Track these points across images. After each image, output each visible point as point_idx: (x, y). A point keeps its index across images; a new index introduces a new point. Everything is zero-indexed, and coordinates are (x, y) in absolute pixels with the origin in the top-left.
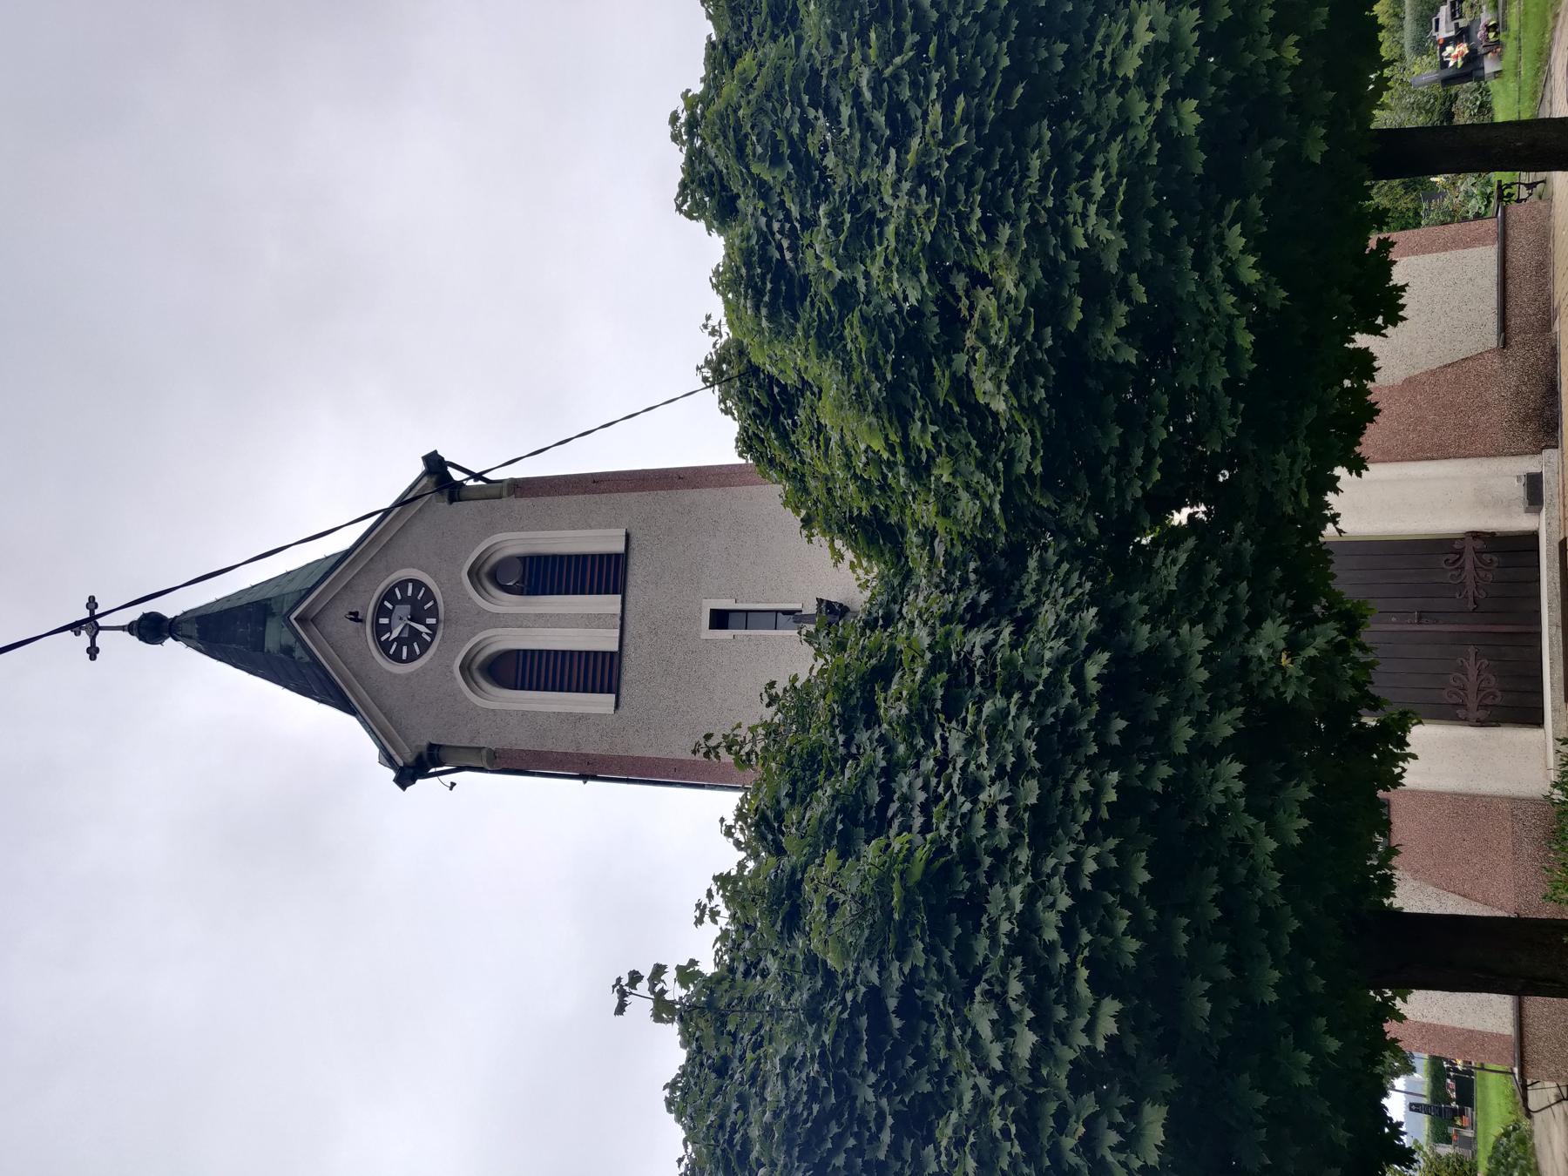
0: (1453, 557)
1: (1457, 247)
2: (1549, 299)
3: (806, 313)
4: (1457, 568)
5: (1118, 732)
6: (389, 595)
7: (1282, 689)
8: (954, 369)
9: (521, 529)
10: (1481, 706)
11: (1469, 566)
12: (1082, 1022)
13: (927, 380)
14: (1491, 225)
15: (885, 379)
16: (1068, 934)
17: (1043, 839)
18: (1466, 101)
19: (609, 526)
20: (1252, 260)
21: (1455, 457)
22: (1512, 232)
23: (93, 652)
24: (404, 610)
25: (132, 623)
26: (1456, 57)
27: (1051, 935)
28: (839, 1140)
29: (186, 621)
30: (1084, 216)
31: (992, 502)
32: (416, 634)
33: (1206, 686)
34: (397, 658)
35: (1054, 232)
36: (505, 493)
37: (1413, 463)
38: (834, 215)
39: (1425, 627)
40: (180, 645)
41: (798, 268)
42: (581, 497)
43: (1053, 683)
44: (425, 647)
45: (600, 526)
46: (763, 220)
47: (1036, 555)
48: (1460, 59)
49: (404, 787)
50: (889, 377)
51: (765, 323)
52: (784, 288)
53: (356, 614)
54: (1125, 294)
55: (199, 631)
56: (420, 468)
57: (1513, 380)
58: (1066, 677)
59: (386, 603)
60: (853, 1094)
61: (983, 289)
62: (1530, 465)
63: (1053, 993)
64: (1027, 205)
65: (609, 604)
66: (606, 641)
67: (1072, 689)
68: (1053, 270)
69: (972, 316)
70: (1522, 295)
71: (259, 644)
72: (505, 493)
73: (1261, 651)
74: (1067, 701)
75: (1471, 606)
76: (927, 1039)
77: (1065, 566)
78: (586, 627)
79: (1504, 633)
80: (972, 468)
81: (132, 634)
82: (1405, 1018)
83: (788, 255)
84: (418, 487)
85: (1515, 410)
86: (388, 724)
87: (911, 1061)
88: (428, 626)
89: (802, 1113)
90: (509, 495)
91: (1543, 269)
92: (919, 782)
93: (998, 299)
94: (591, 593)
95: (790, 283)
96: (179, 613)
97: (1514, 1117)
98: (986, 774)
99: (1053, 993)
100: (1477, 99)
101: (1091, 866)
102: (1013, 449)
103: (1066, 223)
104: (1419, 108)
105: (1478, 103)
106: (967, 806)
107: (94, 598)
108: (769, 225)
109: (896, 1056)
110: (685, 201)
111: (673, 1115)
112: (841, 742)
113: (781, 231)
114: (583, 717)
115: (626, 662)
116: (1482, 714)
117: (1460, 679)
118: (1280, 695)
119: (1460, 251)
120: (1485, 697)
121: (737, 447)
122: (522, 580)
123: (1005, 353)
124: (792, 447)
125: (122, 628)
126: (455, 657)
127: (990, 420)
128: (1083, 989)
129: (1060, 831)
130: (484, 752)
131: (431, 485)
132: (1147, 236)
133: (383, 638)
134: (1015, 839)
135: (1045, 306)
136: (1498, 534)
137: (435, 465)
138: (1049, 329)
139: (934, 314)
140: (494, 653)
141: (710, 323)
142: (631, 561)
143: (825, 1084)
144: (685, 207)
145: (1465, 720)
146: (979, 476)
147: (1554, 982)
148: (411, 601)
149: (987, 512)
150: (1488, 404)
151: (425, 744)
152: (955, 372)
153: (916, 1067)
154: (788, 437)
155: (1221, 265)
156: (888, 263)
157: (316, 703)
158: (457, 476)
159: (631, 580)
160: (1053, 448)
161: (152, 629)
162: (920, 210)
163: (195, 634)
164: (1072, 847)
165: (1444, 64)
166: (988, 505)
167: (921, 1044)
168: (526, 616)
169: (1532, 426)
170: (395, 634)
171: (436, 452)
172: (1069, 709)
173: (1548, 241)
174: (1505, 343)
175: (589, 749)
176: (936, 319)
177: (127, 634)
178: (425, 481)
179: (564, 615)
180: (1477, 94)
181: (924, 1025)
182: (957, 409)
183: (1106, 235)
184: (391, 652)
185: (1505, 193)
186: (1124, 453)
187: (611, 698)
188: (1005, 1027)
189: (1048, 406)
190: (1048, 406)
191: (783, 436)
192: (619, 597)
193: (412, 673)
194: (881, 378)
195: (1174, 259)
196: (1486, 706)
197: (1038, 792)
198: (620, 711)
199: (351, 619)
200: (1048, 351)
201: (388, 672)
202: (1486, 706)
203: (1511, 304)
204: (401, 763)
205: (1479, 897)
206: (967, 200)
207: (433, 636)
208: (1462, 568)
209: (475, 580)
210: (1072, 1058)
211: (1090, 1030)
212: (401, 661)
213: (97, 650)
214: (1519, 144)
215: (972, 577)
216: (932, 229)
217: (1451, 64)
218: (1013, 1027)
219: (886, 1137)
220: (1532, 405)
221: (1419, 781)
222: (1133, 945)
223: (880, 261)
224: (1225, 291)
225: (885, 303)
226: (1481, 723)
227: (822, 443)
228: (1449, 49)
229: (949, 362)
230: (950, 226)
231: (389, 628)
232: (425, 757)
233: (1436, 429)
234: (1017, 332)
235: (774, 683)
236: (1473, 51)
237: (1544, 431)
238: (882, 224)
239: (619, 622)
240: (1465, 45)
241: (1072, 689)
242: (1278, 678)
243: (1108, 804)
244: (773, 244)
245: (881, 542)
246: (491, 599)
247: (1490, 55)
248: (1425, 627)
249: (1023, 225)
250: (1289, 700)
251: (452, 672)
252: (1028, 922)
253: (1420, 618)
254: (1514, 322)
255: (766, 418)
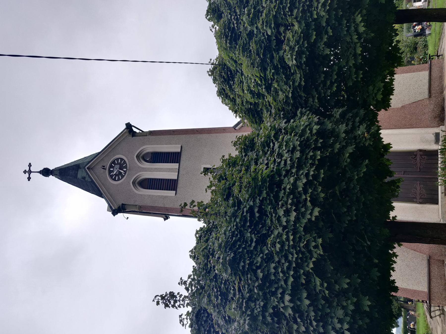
0: (414, 156)
1: (417, 71)
2: (443, 85)
3: (240, 42)
4: (415, 160)
5: (320, 143)
6: (113, 162)
7: (365, 143)
8: (279, 55)
9: (152, 145)
10: (420, 198)
11: (418, 159)
12: (309, 212)
13: (272, 57)
14: (427, 65)
15: (261, 57)
16: (305, 191)
17: (299, 168)
18: (421, 44)
19: (176, 144)
20: (363, 24)
21: (415, 128)
22: (432, 67)
23: (29, 179)
24: (118, 166)
25: (41, 171)
26: (418, 29)
27: (300, 189)
28: (240, 246)
29: (56, 170)
30: (317, 8)
31: (288, 93)
32: (120, 173)
33: (344, 138)
34: (114, 180)
35: (309, 12)
36: (148, 135)
37: (403, 129)
38: (249, 11)
39: (405, 176)
40: (54, 177)
41: (238, 30)
42: (169, 136)
43: (304, 131)
44: (123, 176)
45: (174, 144)
46: (230, 16)
47: (300, 110)
48: (419, 30)
49: (114, 215)
50: (262, 56)
51: (228, 45)
52: (234, 35)
53: (104, 166)
54: (327, 33)
55: (59, 173)
56: (124, 127)
57: (432, 107)
58: (307, 129)
59: (113, 165)
60: (244, 236)
61: (288, 31)
62: (437, 130)
63: (301, 205)
64: (302, 4)
65: (176, 166)
66: (173, 176)
67: (309, 132)
68: (308, 25)
69: (285, 39)
70: (435, 85)
71: (76, 177)
72: (148, 135)
73: (359, 132)
74: (307, 135)
75: (419, 170)
76: (265, 221)
77: (308, 112)
78: (169, 172)
79: (428, 178)
80: (283, 84)
81: (40, 174)
82: (396, 262)
83: (235, 25)
84: (124, 132)
85: (433, 115)
86: (111, 197)
87: (261, 226)
88: (124, 171)
89: (230, 240)
90: (149, 135)
91: (441, 77)
92: (266, 158)
93: (293, 33)
94: (170, 163)
95: (235, 35)
96: (54, 168)
97: (427, 331)
98: (285, 152)
99: (301, 205)
100: (424, 43)
101: (312, 173)
102: (295, 78)
103: (312, 10)
104: (407, 46)
105: (424, 44)
106: (279, 160)
107: (30, 163)
108: (231, 17)
109: (256, 224)
110: (208, 16)
111: (192, 259)
112: (243, 155)
113: (234, 19)
114: (166, 197)
115: (179, 181)
116: (421, 200)
117: (415, 191)
118: (364, 145)
119: (418, 73)
120: (422, 196)
121: (217, 93)
122: (151, 159)
123: (294, 48)
124: (233, 90)
125: (38, 172)
126: (131, 179)
127: (289, 70)
128: (309, 204)
129: (304, 165)
130: (137, 206)
131: (127, 132)
132: (333, 16)
133: (111, 174)
134: (292, 167)
135: (306, 35)
136: (427, 150)
137: (129, 126)
138: (306, 41)
139: (274, 40)
140: (142, 179)
141: (211, 61)
142: (182, 154)
143: (236, 233)
144: (208, 18)
145: (416, 202)
146: (285, 87)
147: (439, 239)
148: (120, 164)
149: (287, 97)
150: (425, 113)
151: (121, 203)
152: (280, 56)
153: (262, 227)
154: (231, 87)
155: (354, 26)
156: (263, 22)
157: (91, 194)
158: (135, 129)
159: (182, 159)
160: (307, 77)
161: (46, 172)
162: (272, 6)
163: (58, 174)
164: (307, 169)
165: (415, 32)
166: (287, 95)
167: (263, 222)
168: (151, 169)
169: (437, 119)
170: (115, 173)
171: (129, 123)
172: (308, 137)
173: (443, 70)
174: (430, 96)
175: (167, 206)
176: (275, 41)
177: (39, 174)
178: (126, 130)
179: (162, 168)
180: (424, 42)
181: (265, 217)
182: (279, 66)
183: (323, 13)
184: (113, 178)
185: (431, 58)
186: (324, 83)
187: (175, 192)
188: (287, 213)
189: (305, 65)
190: (305, 65)
191: (230, 87)
192: (178, 164)
193: (118, 184)
194: (260, 57)
195: (340, 24)
196: (422, 198)
197: (299, 154)
198: (177, 195)
199: (102, 168)
200: (306, 48)
201: (112, 183)
202: (422, 198)
203: (432, 86)
204: (114, 209)
205: (419, 250)
206: (285, 2)
207: (125, 174)
208: (416, 160)
209: (138, 158)
210: (305, 222)
211: (311, 214)
212: (115, 180)
213: (30, 178)
214: (435, 14)
215: (282, 116)
216: (276, 10)
217: (417, 31)
218: (289, 214)
219: (253, 244)
220: (437, 114)
221: (402, 218)
222: (323, 195)
223: (261, 22)
224: (355, 35)
225: (261, 37)
226: (421, 203)
227: (241, 86)
228: (416, 27)
229: (278, 54)
230: (281, 10)
231: (113, 171)
232: (121, 207)
233: (410, 120)
234: (297, 42)
235: (224, 156)
236: (423, 28)
237: (441, 121)
238: (262, 12)
239: (178, 171)
240: (421, 26)
241: (309, 132)
242: (364, 139)
243: (318, 160)
244: (232, 23)
245: (256, 116)
246: (142, 164)
247: (427, 29)
248: (405, 176)
249: (301, 9)
250: (367, 146)
251: (130, 184)
252: (295, 185)
253: (404, 173)
254: (433, 92)
255: (226, 82)
